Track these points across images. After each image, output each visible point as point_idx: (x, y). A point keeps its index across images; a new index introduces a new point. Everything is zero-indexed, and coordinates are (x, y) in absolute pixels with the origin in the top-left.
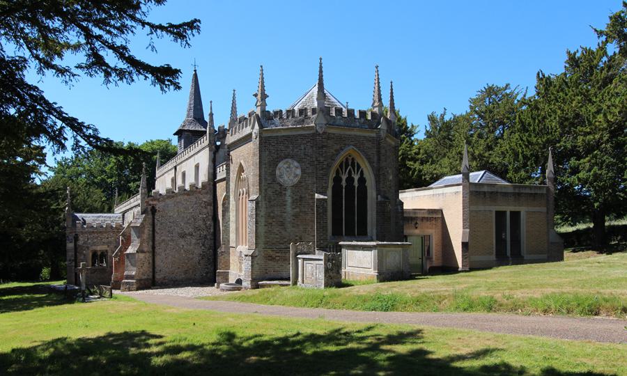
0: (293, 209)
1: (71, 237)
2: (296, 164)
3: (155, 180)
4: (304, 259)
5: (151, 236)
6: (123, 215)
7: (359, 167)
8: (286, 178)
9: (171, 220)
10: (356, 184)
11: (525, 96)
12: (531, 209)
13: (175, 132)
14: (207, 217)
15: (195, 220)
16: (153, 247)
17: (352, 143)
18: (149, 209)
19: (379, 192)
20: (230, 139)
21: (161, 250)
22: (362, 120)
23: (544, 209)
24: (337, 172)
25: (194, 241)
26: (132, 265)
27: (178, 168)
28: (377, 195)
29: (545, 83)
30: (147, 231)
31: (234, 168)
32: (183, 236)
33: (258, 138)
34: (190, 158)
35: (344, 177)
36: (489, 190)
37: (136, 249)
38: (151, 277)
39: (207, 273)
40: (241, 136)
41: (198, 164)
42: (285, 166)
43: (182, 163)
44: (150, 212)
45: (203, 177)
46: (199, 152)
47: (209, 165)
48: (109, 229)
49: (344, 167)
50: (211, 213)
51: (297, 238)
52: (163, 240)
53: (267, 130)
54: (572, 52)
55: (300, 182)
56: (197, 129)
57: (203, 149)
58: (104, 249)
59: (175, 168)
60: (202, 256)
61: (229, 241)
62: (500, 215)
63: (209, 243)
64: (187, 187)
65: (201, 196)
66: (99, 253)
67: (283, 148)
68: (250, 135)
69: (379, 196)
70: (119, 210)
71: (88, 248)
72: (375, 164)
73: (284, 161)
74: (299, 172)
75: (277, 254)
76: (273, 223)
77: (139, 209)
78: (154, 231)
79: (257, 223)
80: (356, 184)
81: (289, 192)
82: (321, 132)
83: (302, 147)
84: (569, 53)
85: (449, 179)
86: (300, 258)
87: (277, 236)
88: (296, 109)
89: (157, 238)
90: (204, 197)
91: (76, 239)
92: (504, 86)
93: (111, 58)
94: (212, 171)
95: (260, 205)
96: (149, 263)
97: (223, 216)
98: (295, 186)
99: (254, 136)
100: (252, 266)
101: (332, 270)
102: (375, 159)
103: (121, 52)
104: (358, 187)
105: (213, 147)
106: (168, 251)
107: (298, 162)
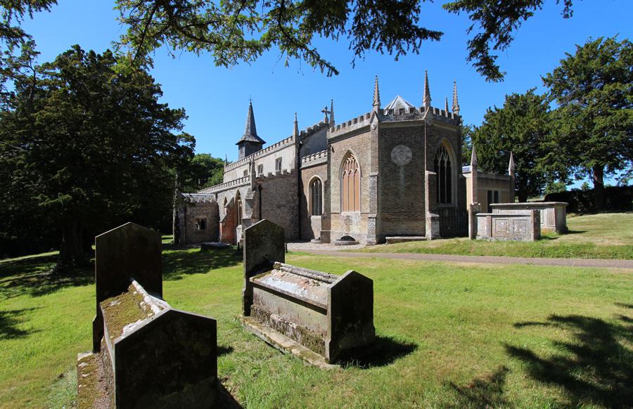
2: (407, 149)
8: (399, 159)
23: (508, 190)
25: (286, 211)
30: (257, 202)
32: (279, 207)
33: (377, 129)
35: (440, 160)
41: (443, 34)
42: (399, 150)
44: (258, 189)
45: (288, 165)
48: (208, 204)
52: (267, 210)
55: (411, 162)
60: (292, 221)
62: (489, 192)
63: (296, 212)
64: (282, 173)
67: (397, 137)
68: (369, 126)
71: (193, 217)
73: (398, 147)
74: (410, 155)
77: (250, 187)
78: (260, 202)
81: (402, 170)
83: (413, 136)
89: (262, 208)
94: (297, 161)
97: (325, 190)
99: (372, 127)
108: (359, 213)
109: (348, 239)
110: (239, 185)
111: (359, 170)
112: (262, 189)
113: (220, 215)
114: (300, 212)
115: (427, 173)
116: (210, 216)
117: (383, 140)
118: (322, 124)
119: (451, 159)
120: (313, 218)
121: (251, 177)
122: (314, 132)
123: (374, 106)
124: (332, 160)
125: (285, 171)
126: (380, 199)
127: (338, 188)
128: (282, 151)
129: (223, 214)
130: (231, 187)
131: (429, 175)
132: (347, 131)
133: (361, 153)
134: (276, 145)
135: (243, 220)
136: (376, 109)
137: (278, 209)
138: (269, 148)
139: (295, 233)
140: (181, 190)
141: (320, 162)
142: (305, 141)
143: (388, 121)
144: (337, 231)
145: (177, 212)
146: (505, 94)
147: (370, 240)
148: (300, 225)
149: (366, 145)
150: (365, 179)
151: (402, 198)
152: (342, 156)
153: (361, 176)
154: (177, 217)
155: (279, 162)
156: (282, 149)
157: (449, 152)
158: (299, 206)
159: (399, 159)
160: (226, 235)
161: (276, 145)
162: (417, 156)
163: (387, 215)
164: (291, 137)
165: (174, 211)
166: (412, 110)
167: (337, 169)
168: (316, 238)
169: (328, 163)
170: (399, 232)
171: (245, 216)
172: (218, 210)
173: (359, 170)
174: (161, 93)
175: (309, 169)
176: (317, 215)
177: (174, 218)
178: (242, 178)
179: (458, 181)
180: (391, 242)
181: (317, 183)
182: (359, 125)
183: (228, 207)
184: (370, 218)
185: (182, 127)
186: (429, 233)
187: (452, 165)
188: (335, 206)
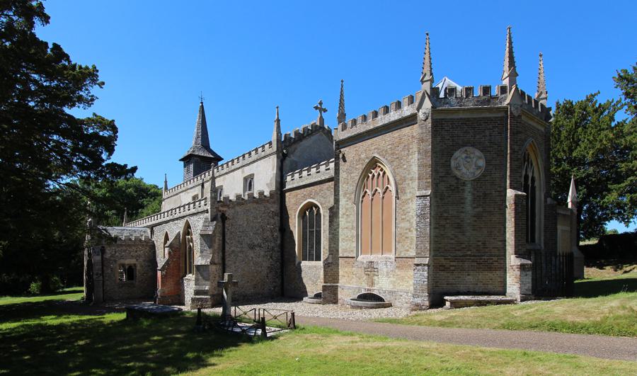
0: (475, 208)
2: (478, 153)
5: (221, 246)
8: (464, 170)
9: (241, 230)
14: (274, 228)
16: (223, 259)
18: (219, 216)
21: (230, 262)
26: (204, 278)
27: (205, 185)
28: (545, 198)
30: (218, 238)
32: (252, 247)
33: (429, 120)
37: (209, 260)
39: (275, 287)
41: (253, 174)
44: (220, 219)
48: (138, 243)
51: (480, 243)
52: (233, 251)
53: (442, 110)
55: (483, 175)
56: (205, 155)
58: (132, 263)
60: (270, 269)
61: (338, 251)
63: (277, 255)
65: (269, 205)
69: (549, 199)
71: (115, 261)
74: (482, 163)
75: (452, 264)
76: (448, 226)
77: (208, 215)
81: (468, 188)
82: (517, 115)
83: (487, 133)
87: (453, 241)
89: (227, 249)
90: (272, 207)
94: (279, 180)
98: (477, 180)
99: (421, 115)
105: (281, 154)
106: (237, 264)
107: (482, 151)
108: (392, 256)
109: (371, 299)
110: (188, 212)
111: (392, 188)
112: (226, 218)
113: (158, 259)
114: (282, 256)
115: (510, 193)
116: (141, 260)
117: (439, 139)
118: (314, 126)
119: (536, 175)
120: (304, 264)
121: (209, 200)
122: (304, 137)
123: (422, 81)
124: (343, 175)
125: (261, 193)
126: (432, 235)
127: (353, 218)
128: (255, 164)
129: (162, 258)
130: (176, 216)
131: (516, 196)
132: (380, 124)
133: (397, 160)
134: (244, 156)
135: (198, 267)
136: (426, 86)
137: (250, 251)
138: (233, 161)
139: (275, 287)
140: (101, 218)
141: (319, 179)
142: (291, 149)
143: (446, 107)
144: (350, 285)
145: (89, 255)
146: (556, 100)
147: (418, 301)
148: (282, 272)
149: (407, 147)
150: (406, 202)
151: (468, 234)
152: (361, 167)
153: (397, 198)
154: (89, 262)
155: (249, 182)
156: (254, 162)
157: (534, 164)
158: (282, 246)
159: (464, 170)
160: (166, 290)
161: (244, 156)
162: (494, 163)
163: (443, 261)
164: (270, 143)
165: (86, 252)
166: (486, 90)
167: (352, 188)
168: (311, 294)
169: (335, 179)
170: (462, 288)
171: (199, 260)
172: (155, 252)
173: (392, 188)
174: (46, 19)
175: (298, 191)
176: (311, 259)
177: (85, 263)
178: (189, 204)
179: (545, 207)
180: (455, 305)
181: (311, 212)
182: (394, 116)
183: (170, 246)
184: (418, 265)
185: (92, 100)
186: (513, 287)
187: (536, 184)
188: (346, 245)
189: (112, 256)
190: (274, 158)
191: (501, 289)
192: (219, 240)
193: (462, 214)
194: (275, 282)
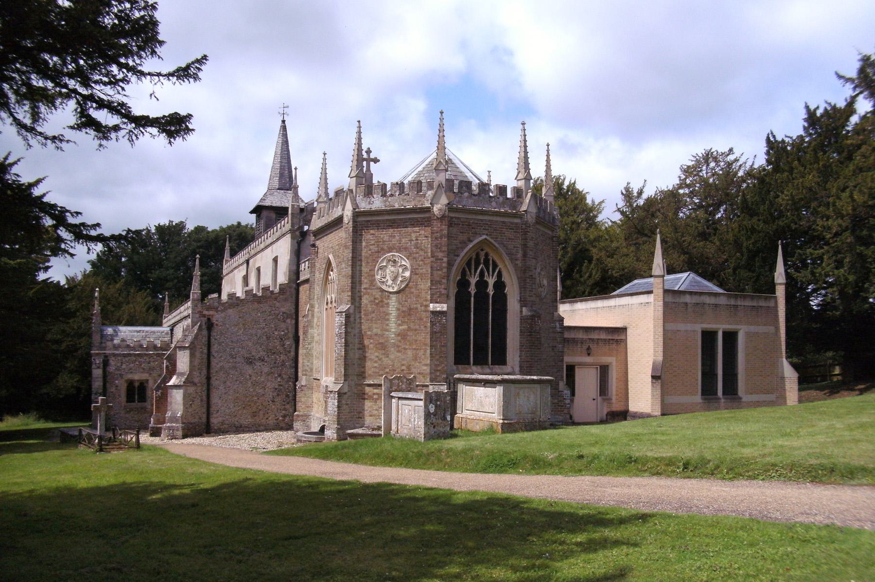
0: (400, 325)
1: (98, 361)
3: (222, 279)
4: (400, 398)
5: (205, 360)
6: (172, 330)
7: (495, 266)
9: (235, 339)
10: (491, 290)
11: (753, 164)
12: (753, 328)
13: (252, 208)
15: (268, 338)
16: (208, 378)
17: (486, 232)
19: (523, 302)
20: (316, 223)
22: (501, 199)
24: (464, 274)
27: (251, 261)
28: (521, 307)
29: (774, 146)
31: (320, 265)
32: (250, 361)
34: (266, 247)
35: (473, 280)
36: (694, 301)
37: (183, 380)
38: (204, 420)
40: (330, 220)
43: (256, 255)
46: (278, 239)
47: (290, 260)
49: (473, 267)
50: (292, 330)
51: (404, 368)
54: (812, 108)
57: (283, 235)
59: (247, 262)
62: (708, 337)
65: (278, 304)
66: (137, 384)
67: (386, 238)
70: (169, 320)
71: (121, 375)
72: (518, 262)
79: (347, 344)
80: (491, 290)
84: (807, 107)
85: (639, 284)
86: (394, 397)
87: (376, 365)
88: (406, 182)
89: (214, 362)
91: (106, 363)
92: (726, 150)
93: (103, 117)
94: (294, 268)
95: (352, 319)
96: (202, 400)
99: (346, 220)
100: (339, 407)
101: (435, 414)
102: (520, 255)
103: (120, 110)
104: (476, 294)
105: (298, 233)
119: (506, 278)
151: (392, 357)
189: (118, 369)
190: (288, 238)
191: (221, 412)
192: (202, 352)
193: (387, 333)
194: (285, 409)
